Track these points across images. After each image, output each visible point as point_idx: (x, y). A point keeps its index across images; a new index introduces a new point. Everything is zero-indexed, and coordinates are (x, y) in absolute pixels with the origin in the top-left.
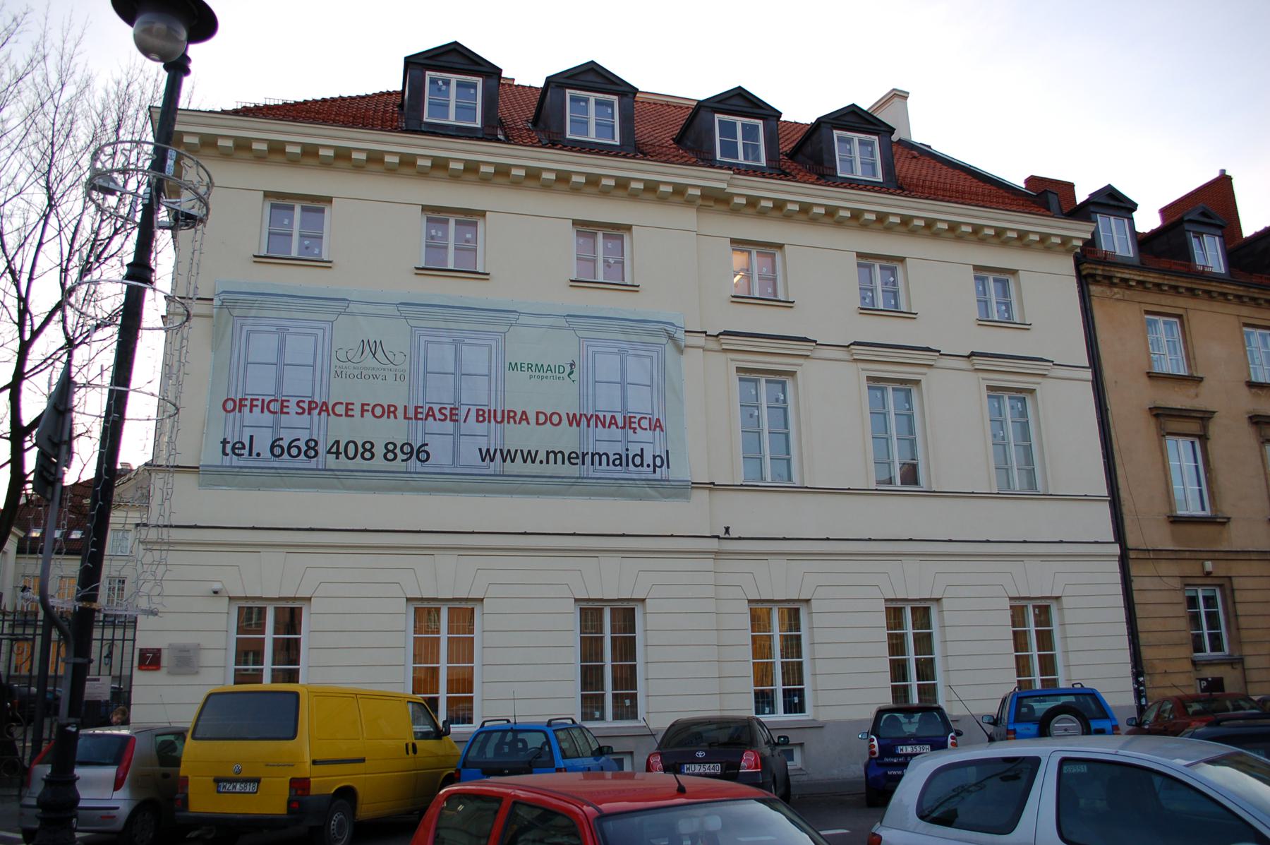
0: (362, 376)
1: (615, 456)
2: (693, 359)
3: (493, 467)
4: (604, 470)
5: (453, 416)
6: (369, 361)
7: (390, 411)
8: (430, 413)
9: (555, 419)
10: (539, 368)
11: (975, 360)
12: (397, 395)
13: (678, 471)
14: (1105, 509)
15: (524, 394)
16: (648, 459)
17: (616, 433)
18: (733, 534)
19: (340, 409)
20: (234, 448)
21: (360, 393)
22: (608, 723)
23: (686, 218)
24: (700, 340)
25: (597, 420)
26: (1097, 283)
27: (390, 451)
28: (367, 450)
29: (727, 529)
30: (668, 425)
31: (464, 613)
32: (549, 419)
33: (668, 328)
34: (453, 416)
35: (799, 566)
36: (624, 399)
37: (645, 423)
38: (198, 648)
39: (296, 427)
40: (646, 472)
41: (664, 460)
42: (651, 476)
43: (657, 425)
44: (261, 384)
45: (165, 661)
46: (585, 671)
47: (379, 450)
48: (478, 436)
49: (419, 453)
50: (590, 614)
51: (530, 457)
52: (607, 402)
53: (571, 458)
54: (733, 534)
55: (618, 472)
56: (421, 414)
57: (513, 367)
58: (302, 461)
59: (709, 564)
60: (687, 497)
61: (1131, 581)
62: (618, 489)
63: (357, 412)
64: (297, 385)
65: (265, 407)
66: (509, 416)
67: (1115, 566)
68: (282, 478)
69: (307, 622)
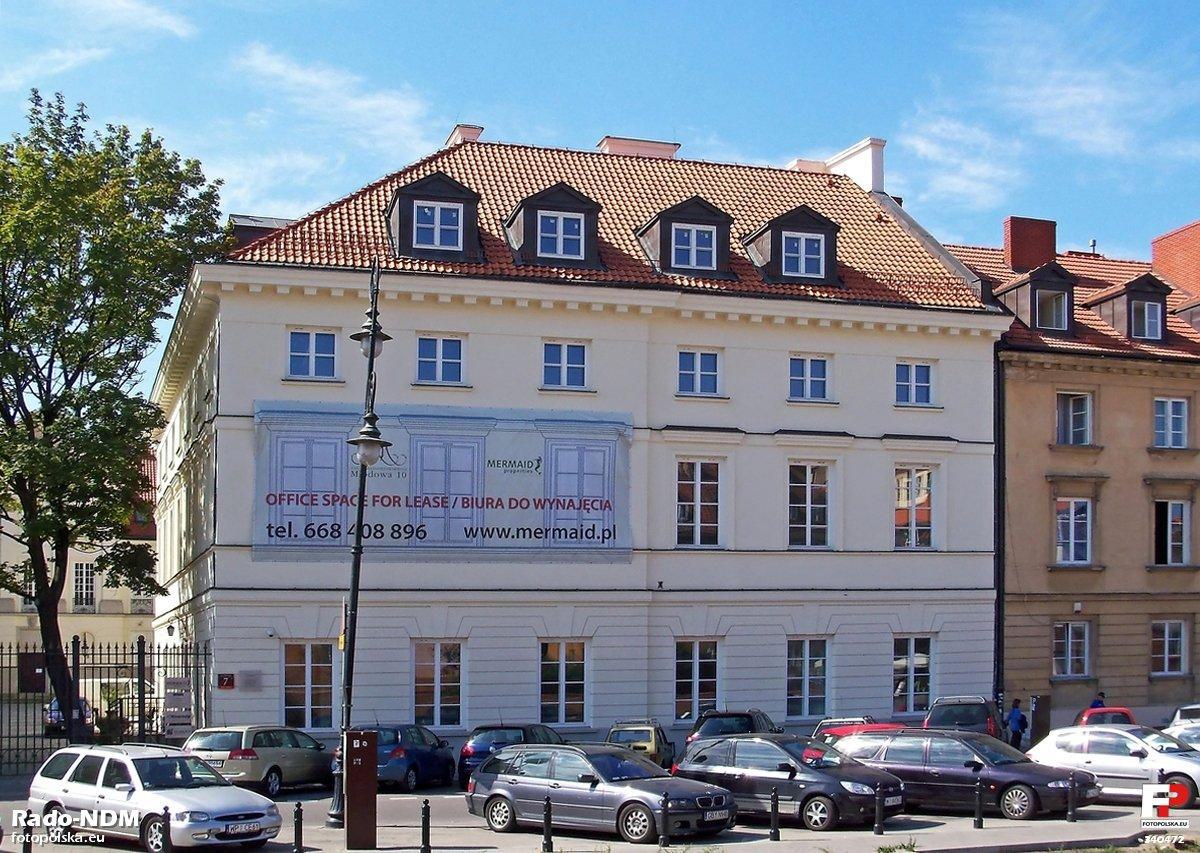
5: (444, 503)
8: (426, 501)
9: (525, 504)
16: (598, 532)
17: (573, 513)
27: (396, 531)
29: (661, 583)
32: (519, 503)
34: (444, 503)
36: (580, 487)
37: (597, 505)
40: (596, 542)
42: (601, 546)
43: (606, 505)
44: (295, 483)
47: (387, 531)
48: (463, 518)
49: (418, 532)
52: (567, 488)
56: (418, 502)
66: (488, 502)
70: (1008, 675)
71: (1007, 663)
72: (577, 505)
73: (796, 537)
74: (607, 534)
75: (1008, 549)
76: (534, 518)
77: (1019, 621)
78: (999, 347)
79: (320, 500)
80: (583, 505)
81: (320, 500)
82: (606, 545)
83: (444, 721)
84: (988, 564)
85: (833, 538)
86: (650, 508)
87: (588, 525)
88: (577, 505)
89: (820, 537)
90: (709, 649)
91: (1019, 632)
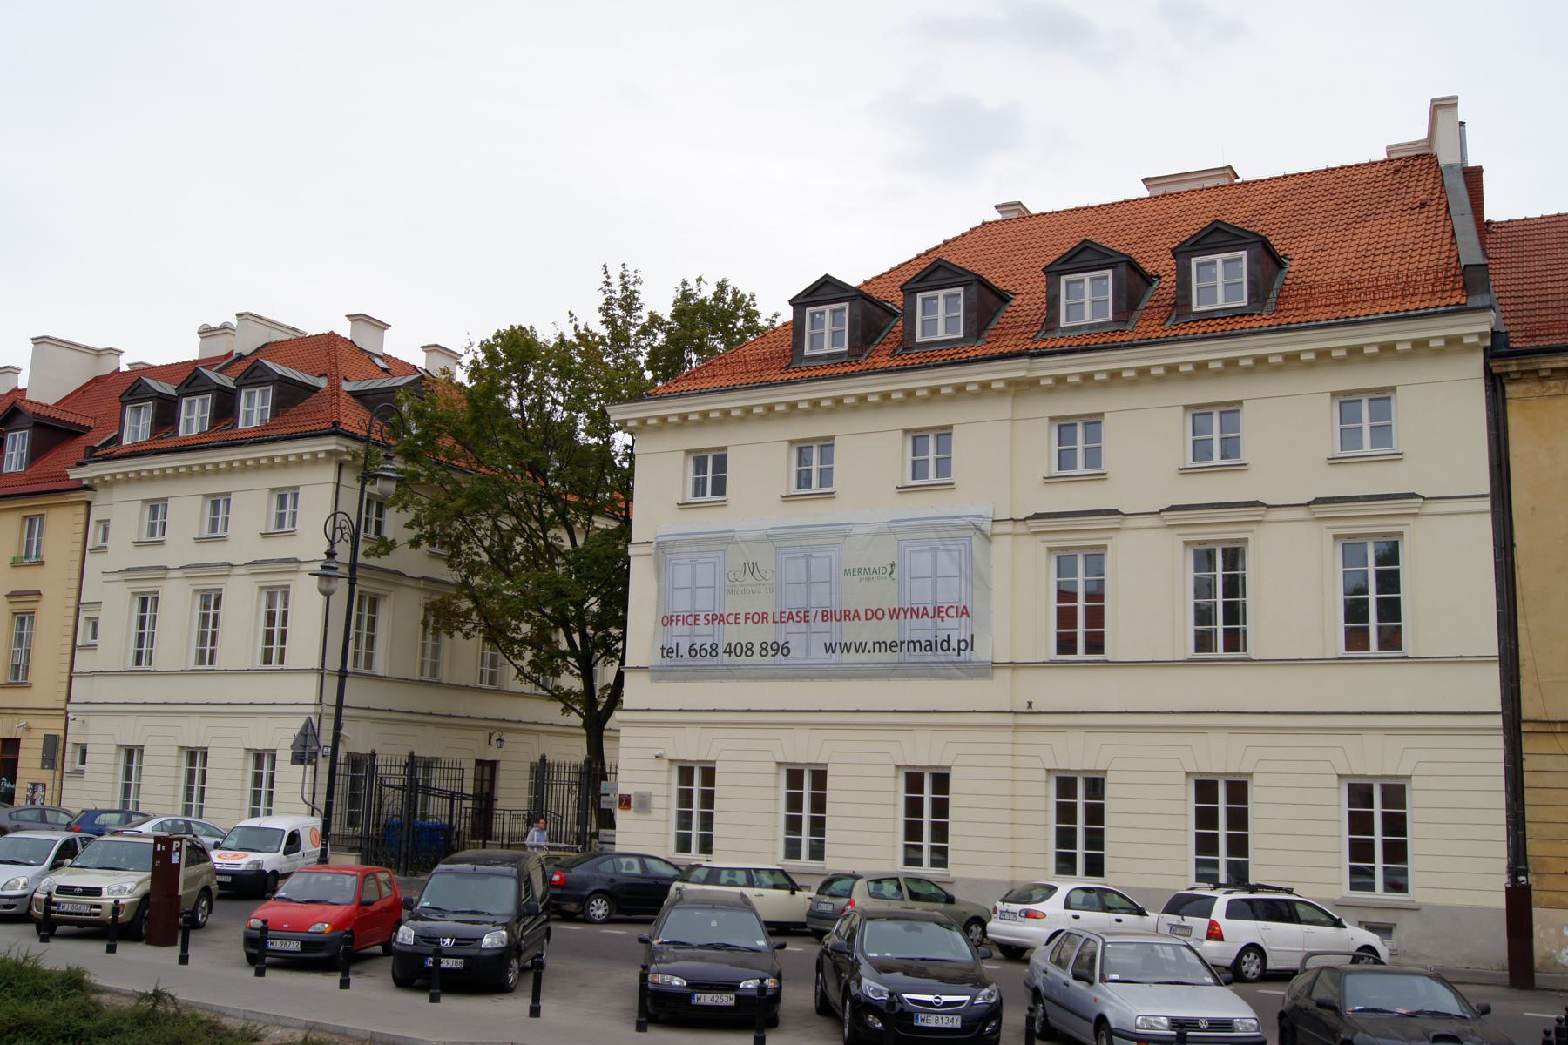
0: (745, 592)
1: (932, 643)
2: (1001, 547)
3: (835, 657)
4: (917, 656)
5: (806, 618)
6: (750, 580)
7: (763, 617)
8: (791, 617)
9: (880, 614)
10: (867, 571)
11: (1314, 508)
12: (766, 604)
13: (981, 653)
14: (1493, 674)
15: (858, 595)
16: (954, 644)
17: (928, 622)
18: (484, 736)
19: (732, 619)
20: (668, 652)
21: (742, 605)
22: (805, 862)
23: (1003, 408)
24: (1008, 527)
25: (914, 612)
26: (1515, 381)
27: (764, 647)
28: (748, 649)
29: (1030, 704)
30: (975, 610)
31: (493, 765)
32: (875, 614)
33: (977, 521)
34: (806, 618)
35: (1096, 739)
36: (934, 591)
37: (952, 612)
38: (650, 795)
39: (705, 634)
40: (952, 655)
41: (969, 644)
42: (956, 659)
43: (964, 612)
44: (682, 605)
45: (633, 803)
46: (1244, 852)
47: (757, 648)
48: (824, 632)
49: (782, 649)
50: (1360, 794)
51: (861, 648)
52: (922, 595)
53: (893, 646)
54: (1035, 709)
55: (929, 656)
56: (784, 618)
57: (847, 572)
58: (708, 661)
59: (1007, 736)
60: (991, 677)
61: (1522, 760)
62: (930, 672)
63: (742, 620)
64: (705, 605)
65: (685, 620)
66: (846, 615)
67: (1498, 742)
68: (698, 674)
69: (1253, 794)
70: (1533, 848)
71: (1531, 829)
72: (931, 613)
73: (1066, 644)
74: (963, 645)
75: (1524, 652)
76: (888, 630)
77: (1550, 763)
78: (1490, 355)
79: (702, 620)
80: (938, 612)
81: (702, 620)
82: (962, 658)
83: (934, 864)
84: (1491, 677)
85: (1410, 644)
86: (1019, 611)
87: (942, 636)
88: (931, 613)
89: (1095, 644)
90: (1395, 793)
91: (1549, 780)
